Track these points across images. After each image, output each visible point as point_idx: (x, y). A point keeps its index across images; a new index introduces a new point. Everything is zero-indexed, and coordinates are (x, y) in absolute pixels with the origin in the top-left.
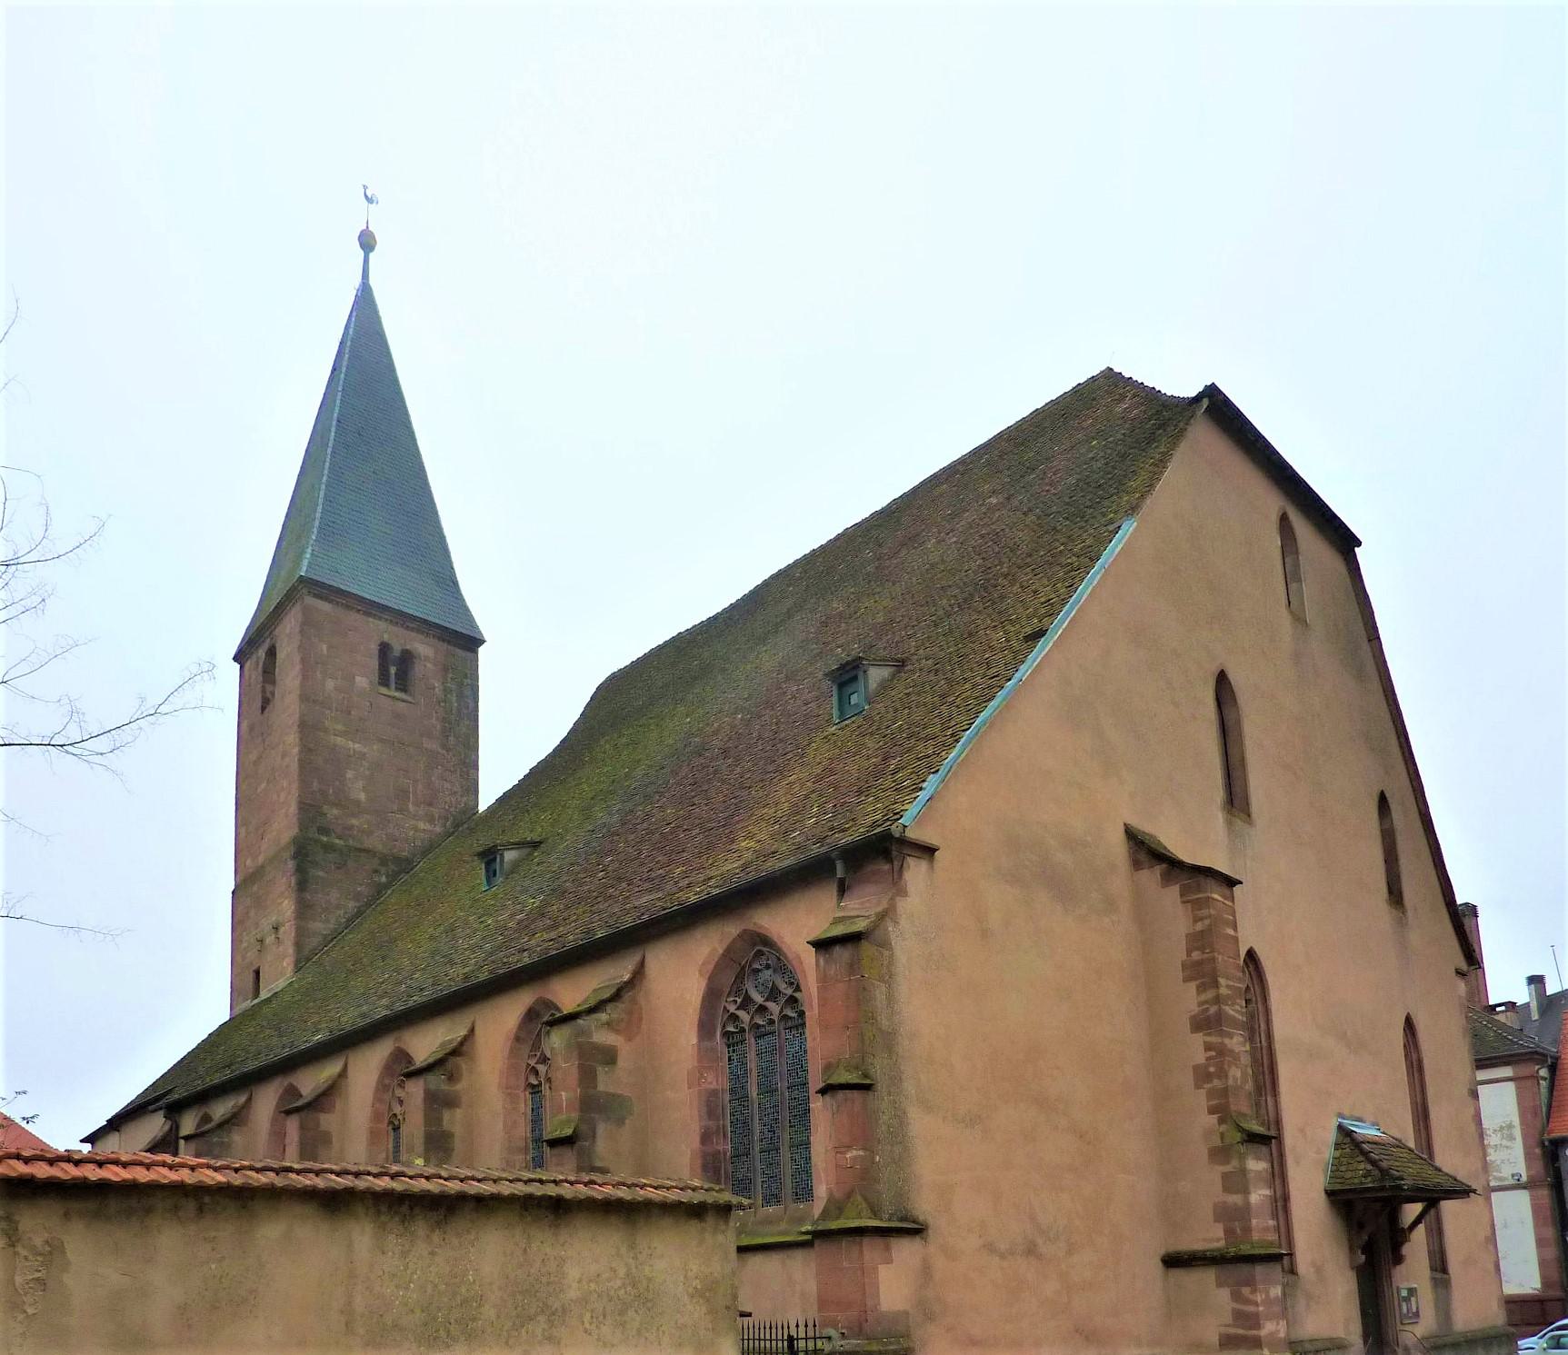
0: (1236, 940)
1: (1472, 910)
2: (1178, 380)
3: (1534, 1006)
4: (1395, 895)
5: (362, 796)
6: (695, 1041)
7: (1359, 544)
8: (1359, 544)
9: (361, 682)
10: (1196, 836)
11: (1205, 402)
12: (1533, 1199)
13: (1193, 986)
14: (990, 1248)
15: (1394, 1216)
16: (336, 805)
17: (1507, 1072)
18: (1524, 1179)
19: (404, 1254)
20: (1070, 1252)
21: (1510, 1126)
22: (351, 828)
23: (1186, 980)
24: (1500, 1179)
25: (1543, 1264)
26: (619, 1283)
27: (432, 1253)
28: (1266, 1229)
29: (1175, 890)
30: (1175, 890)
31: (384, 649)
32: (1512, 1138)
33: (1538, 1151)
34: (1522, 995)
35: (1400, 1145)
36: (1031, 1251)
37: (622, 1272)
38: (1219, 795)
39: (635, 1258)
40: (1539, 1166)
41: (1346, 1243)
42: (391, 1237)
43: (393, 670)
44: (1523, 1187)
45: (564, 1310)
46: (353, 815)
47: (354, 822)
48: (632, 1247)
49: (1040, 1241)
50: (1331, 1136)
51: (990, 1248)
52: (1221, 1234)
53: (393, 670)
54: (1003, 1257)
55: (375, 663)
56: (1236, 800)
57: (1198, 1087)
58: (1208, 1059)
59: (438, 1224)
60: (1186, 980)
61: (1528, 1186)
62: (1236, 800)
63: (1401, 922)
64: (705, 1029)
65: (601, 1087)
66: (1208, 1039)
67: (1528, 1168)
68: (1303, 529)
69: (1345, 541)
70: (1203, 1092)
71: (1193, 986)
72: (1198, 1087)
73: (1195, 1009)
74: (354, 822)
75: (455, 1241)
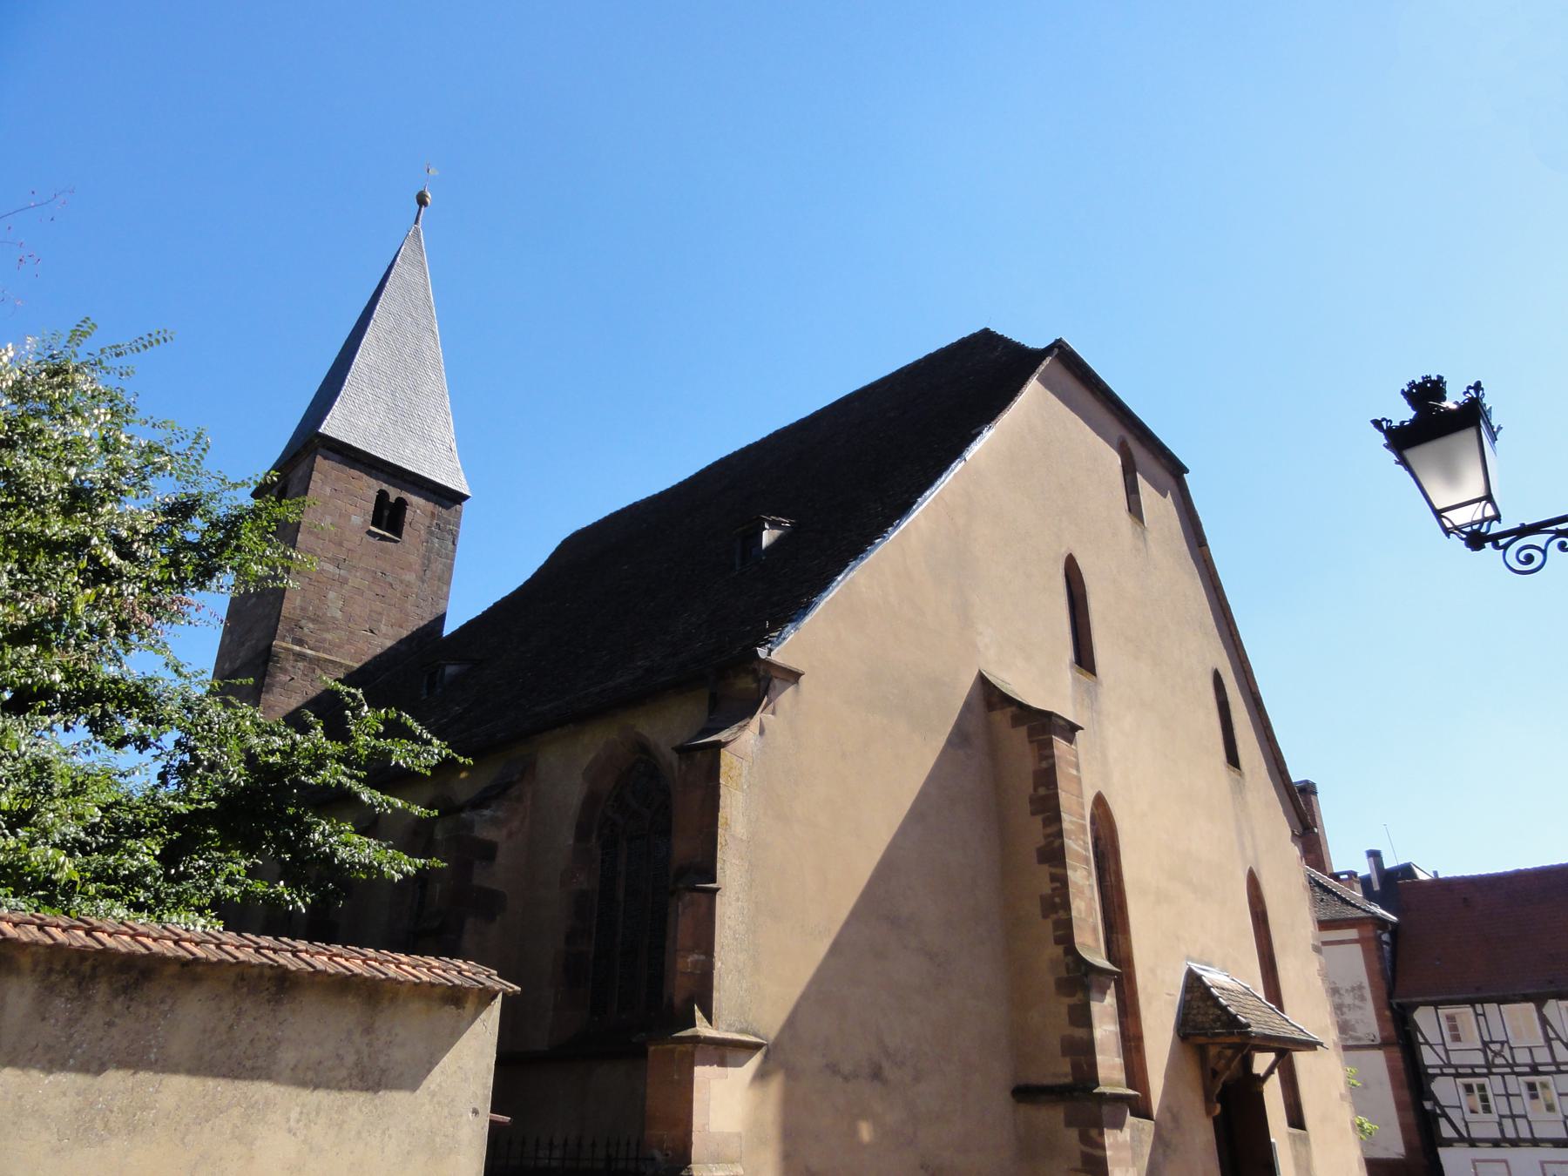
0: (1079, 780)
1: (1308, 789)
2: (1035, 339)
3: (1375, 878)
4: (1233, 759)
5: (339, 614)
6: (571, 842)
7: (1187, 471)
8: (1187, 471)
9: (357, 520)
10: (1041, 681)
11: (1056, 351)
12: (1389, 1060)
13: (1039, 819)
14: (833, 1069)
15: (1247, 1063)
16: (313, 621)
17: (1352, 933)
18: (1378, 1041)
19: (72, 1022)
20: (917, 1079)
21: (1360, 987)
22: (324, 640)
23: (1033, 814)
24: (1359, 1039)
25: (1404, 1128)
26: (344, 1073)
27: (110, 1024)
28: (1113, 1067)
29: (1023, 731)
30: (1023, 731)
31: (382, 496)
32: (1363, 998)
33: (1388, 1013)
34: (1364, 868)
35: (1248, 993)
36: (877, 1074)
37: (350, 1059)
38: (1068, 654)
39: (370, 1045)
40: (1391, 1030)
41: (1200, 1092)
42: (59, 1003)
43: (386, 513)
44: (1378, 1047)
45: (266, 1103)
46: (328, 630)
47: (328, 636)
48: (368, 1030)
49: (886, 1065)
50: (1180, 981)
51: (833, 1069)
52: (1067, 1068)
53: (386, 513)
54: (846, 1079)
55: (371, 507)
56: (1084, 658)
57: (1045, 916)
58: (1054, 889)
59: (125, 990)
60: (1033, 814)
61: (1384, 1045)
62: (1084, 658)
63: (1239, 789)
64: (582, 832)
65: (476, 881)
66: (1054, 870)
67: (1382, 1029)
68: (1140, 453)
69: (1174, 470)
70: (1049, 923)
71: (1039, 819)
72: (1045, 916)
73: (1041, 841)
74: (328, 636)
75: (144, 1010)
